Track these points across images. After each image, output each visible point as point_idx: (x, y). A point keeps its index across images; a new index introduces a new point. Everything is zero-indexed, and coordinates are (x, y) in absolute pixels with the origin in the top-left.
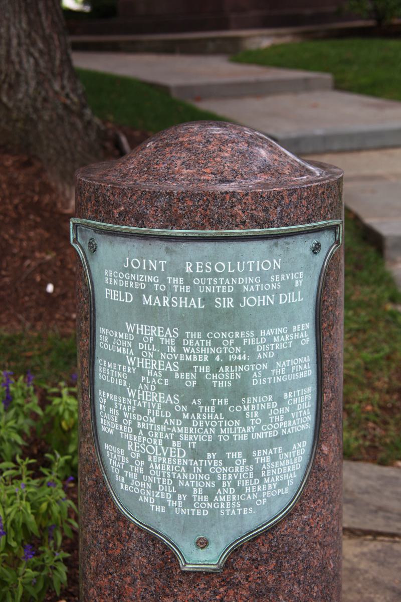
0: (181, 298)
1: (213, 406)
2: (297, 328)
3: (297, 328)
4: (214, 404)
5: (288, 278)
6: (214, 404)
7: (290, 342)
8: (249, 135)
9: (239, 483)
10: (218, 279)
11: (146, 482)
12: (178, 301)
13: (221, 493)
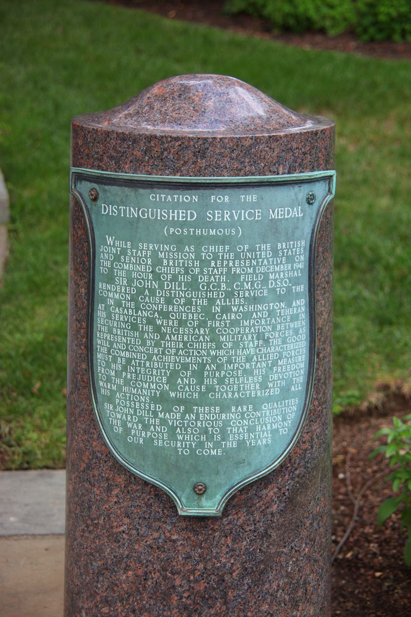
0: (171, 211)
1: (194, 305)
2: (281, 327)
3: (281, 327)
4: (194, 304)
5: (252, 295)
6: (194, 304)
7: (270, 362)
8: (317, 359)
9: (233, 270)
10: (118, 208)
11: (129, 408)
12: (168, 214)
13: (220, 304)
